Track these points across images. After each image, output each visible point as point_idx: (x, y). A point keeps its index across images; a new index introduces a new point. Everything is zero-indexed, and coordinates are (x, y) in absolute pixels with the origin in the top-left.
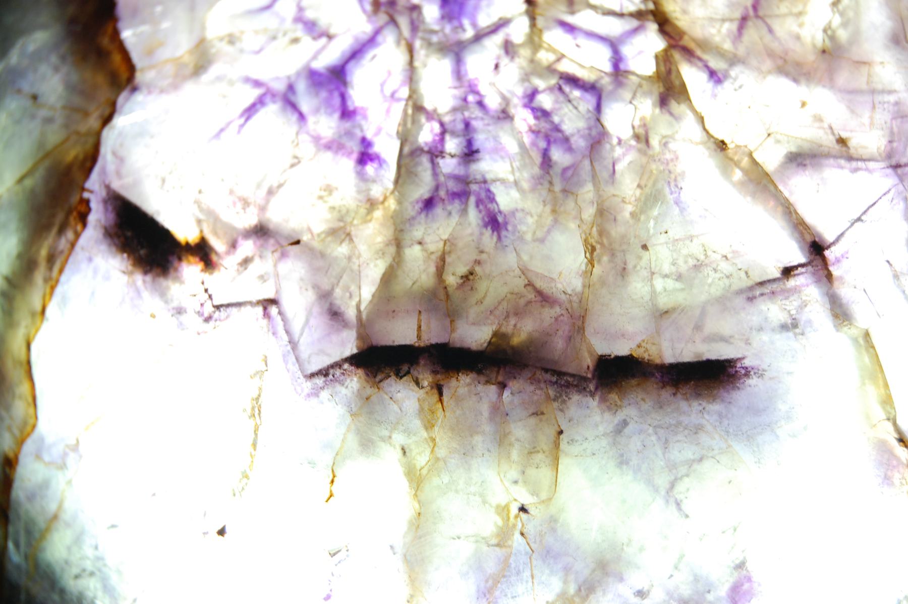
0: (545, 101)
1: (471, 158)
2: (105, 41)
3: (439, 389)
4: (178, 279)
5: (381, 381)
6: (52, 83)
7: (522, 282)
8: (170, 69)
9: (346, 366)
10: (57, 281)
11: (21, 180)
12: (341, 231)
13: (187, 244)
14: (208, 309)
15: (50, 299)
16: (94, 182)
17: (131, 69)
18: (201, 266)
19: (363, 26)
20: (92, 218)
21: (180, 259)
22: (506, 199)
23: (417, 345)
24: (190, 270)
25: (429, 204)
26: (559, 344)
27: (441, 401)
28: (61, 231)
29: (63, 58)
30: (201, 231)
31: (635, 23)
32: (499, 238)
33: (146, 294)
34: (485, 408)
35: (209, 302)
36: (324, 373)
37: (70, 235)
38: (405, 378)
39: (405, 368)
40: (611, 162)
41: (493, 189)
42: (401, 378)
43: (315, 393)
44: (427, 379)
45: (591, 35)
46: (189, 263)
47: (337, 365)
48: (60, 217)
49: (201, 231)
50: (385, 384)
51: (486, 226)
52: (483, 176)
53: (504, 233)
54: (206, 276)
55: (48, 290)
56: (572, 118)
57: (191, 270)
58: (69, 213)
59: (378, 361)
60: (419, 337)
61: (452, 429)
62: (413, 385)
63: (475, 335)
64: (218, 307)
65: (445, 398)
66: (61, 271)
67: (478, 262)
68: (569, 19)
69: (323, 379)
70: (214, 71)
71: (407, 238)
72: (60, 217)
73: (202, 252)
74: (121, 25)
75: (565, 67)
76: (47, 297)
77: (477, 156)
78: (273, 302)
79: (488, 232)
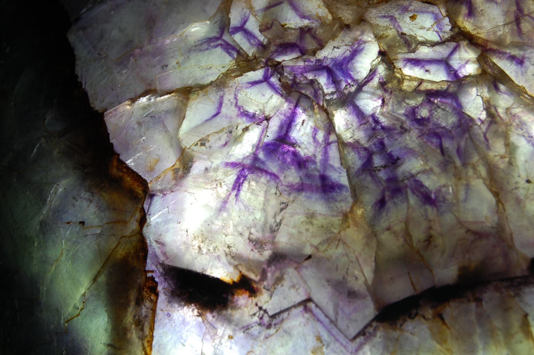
0: (424, 113)
1: (396, 164)
2: (114, 171)
3: (440, 317)
4: (235, 307)
5: (401, 325)
6: (89, 210)
7: (462, 231)
8: (170, 175)
9: (374, 324)
10: (152, 337)
11: (95, 280)
12: (333, 239)
13: (234, 282)
14: (266, 319)
15: (151, 350)
16: (150, 265)
17: (144, 183)
18: (247, 294)
19: (286, 107)
20: (160, 288)
21: (233, 295)
22: (430, 183)
23: (415, 294)
24: (242, 299)
25: (381, 203)
26: (499, 261)
27: (444, 323)
28: (139, 302)
29: (89, 190)
30: (240, 272)
31: (453, 44)
32: (438, 210)
33: (218, 325)
34: (473, 317)
35: (266, 315)
36: (362, 333)
37: (148, 304)
38: (416, 318)
39: (414, 311)
40: (482, 135)
41: (417, 178)
42: (413, 318)
43: (360, 347)
44: (429, 313)
45: (431, 61)
46: (239, 294)
47: (369, 325)
48: (133, 295)
49: (240, 272)
50: (404, 327)
51: (424, 204)
52: (410, 173)
53: (438, 204)
54: (255, 300)
55: (146, 345)
56: (446, 119)
57: (242, 299)
58: (140, 290)
59: (391, 315)
60: (414, 288)
61: (457, 339)
62: (423, 320)
63: (447, 273)
64: (273, 317)
65: (447, 321)
66: (152, 329)
67: (430, 228)
68: (412, 56)
69: (362, 338)
70: (198, 167)
71: (378, 229)
72: (133, 295)
73: (245, 285)
74: (122, 158)
75: (426, 86)
76: (148, 349)
77: (399, 162)
78: (309, 300)
79: (429, 208)
